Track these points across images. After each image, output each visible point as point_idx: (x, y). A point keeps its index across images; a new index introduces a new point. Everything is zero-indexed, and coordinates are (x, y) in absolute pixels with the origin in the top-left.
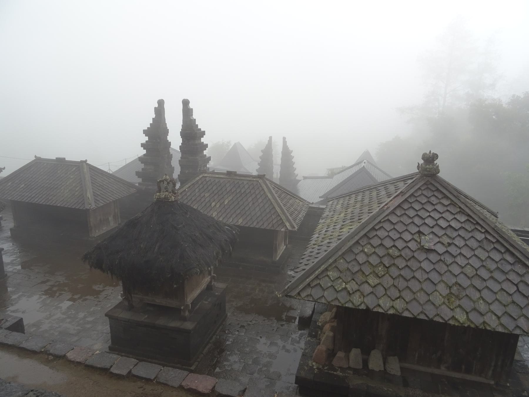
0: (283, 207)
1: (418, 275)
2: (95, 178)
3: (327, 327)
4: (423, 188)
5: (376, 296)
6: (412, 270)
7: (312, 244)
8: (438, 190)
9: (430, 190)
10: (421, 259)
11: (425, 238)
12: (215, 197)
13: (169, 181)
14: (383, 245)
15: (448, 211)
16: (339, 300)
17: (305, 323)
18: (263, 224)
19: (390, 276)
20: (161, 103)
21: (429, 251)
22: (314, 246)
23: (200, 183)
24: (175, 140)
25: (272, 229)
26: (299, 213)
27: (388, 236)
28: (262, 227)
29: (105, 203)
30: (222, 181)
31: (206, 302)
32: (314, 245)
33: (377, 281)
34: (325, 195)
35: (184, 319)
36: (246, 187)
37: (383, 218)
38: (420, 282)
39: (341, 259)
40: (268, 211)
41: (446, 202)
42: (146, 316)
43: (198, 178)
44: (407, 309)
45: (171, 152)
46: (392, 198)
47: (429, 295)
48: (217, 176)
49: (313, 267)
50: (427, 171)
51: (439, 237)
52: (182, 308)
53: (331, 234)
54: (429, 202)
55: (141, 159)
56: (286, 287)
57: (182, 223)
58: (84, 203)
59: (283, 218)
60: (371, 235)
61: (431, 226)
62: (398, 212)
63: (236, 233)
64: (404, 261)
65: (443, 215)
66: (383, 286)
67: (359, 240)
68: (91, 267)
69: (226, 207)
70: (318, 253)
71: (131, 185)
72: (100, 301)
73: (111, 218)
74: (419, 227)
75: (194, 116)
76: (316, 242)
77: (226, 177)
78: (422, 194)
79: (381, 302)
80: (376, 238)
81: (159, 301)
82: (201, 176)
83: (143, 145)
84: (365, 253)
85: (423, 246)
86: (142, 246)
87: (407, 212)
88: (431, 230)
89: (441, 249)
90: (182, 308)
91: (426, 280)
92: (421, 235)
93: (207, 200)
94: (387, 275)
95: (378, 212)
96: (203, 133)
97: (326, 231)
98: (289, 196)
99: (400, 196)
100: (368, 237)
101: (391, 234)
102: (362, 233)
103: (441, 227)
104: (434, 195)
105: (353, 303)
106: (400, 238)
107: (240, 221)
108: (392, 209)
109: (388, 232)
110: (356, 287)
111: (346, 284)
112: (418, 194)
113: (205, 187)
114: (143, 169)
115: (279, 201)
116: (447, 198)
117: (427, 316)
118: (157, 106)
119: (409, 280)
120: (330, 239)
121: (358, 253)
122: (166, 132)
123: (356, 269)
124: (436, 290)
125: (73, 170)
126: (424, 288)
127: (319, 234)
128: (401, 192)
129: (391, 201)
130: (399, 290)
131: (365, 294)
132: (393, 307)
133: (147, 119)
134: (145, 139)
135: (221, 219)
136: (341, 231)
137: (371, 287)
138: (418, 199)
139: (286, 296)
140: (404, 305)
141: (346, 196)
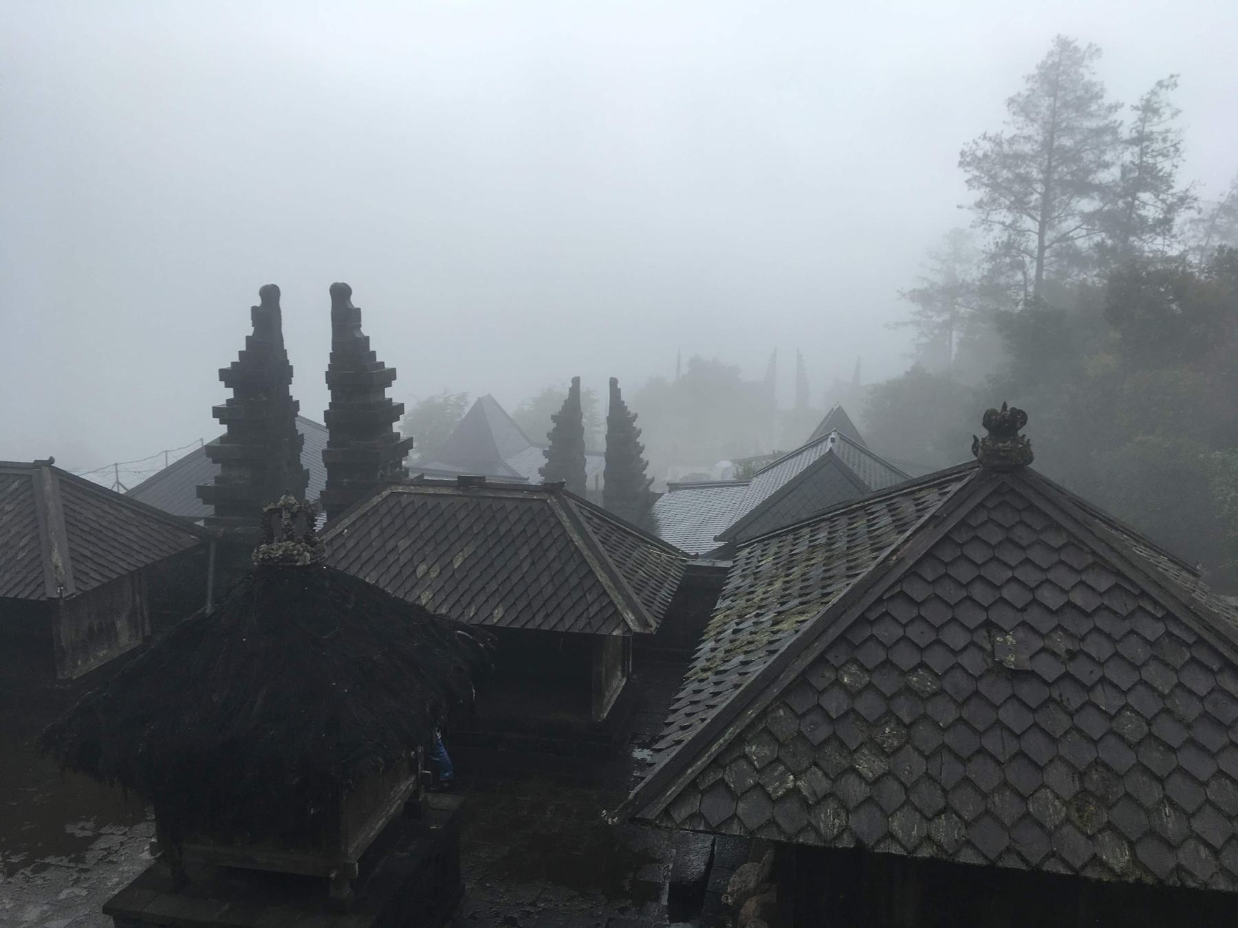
1: (991, 743)
5: (881, 809)
8: (1031, 507)
10: (998, 700)
11: (1005, 641)
14: (892, 665)
15: (1062, 562)
16: (778, 826)
19: (916, 749)
20: (270, 295)
21: (1018, 675)
22: (705, 675)
24: (311, 396)
25: (588, 631)
26: (660, 584)
27: (905, 638)
28: (560, 629)
29: (106, 581)
32: (704, 670)
33: (880, 766)
34: (728, 531)
38: (999, 763)
41: (1057, 540)
43: (377, 500)
44: (968, 843)
45: (300, 428)
48: (431, 491)
51: (1042, 636)
55: (212, 451)
59: (618, 599)
62: (929, 573)
65: (1051, 576)
66: (898, 779)
69: (458, 576)
70: (715, 694)
71: (186, 525)
73: (121, 624)
75: (365, 330)
77: (456, 493)
79: (895, 825)
82: (385, 493)
83: (217, 412)
84: (844, 687)
85: (1001, 662)
89: (1049, 669)
91: (1014, 757)
92: (994, 632)
96: (391, 375)
97: (735, 632)
99: (931, 527)
101: (914, 632)
102: (834, 633)
103: (1047, 608)
104: (1021, 522)
105: (816, 830)
106: (937, 642)
107: (498, 613)
108: (911, 562)
109: (905, 626)
110: (824, 785)
111: (796, 779)
115: (605, 554)
116: (1059, 528)
118: (258, 302)
119: (969, 760)
122: (286, 373)
123: (823, 733)
127: (717, 641)
128: (933, 517)
129: (907, 541)
130: (944, 790)
131: (851, 806)
132: (929, 838)
133: (232, 339)
135: (443, 611)
137: (867, 783)
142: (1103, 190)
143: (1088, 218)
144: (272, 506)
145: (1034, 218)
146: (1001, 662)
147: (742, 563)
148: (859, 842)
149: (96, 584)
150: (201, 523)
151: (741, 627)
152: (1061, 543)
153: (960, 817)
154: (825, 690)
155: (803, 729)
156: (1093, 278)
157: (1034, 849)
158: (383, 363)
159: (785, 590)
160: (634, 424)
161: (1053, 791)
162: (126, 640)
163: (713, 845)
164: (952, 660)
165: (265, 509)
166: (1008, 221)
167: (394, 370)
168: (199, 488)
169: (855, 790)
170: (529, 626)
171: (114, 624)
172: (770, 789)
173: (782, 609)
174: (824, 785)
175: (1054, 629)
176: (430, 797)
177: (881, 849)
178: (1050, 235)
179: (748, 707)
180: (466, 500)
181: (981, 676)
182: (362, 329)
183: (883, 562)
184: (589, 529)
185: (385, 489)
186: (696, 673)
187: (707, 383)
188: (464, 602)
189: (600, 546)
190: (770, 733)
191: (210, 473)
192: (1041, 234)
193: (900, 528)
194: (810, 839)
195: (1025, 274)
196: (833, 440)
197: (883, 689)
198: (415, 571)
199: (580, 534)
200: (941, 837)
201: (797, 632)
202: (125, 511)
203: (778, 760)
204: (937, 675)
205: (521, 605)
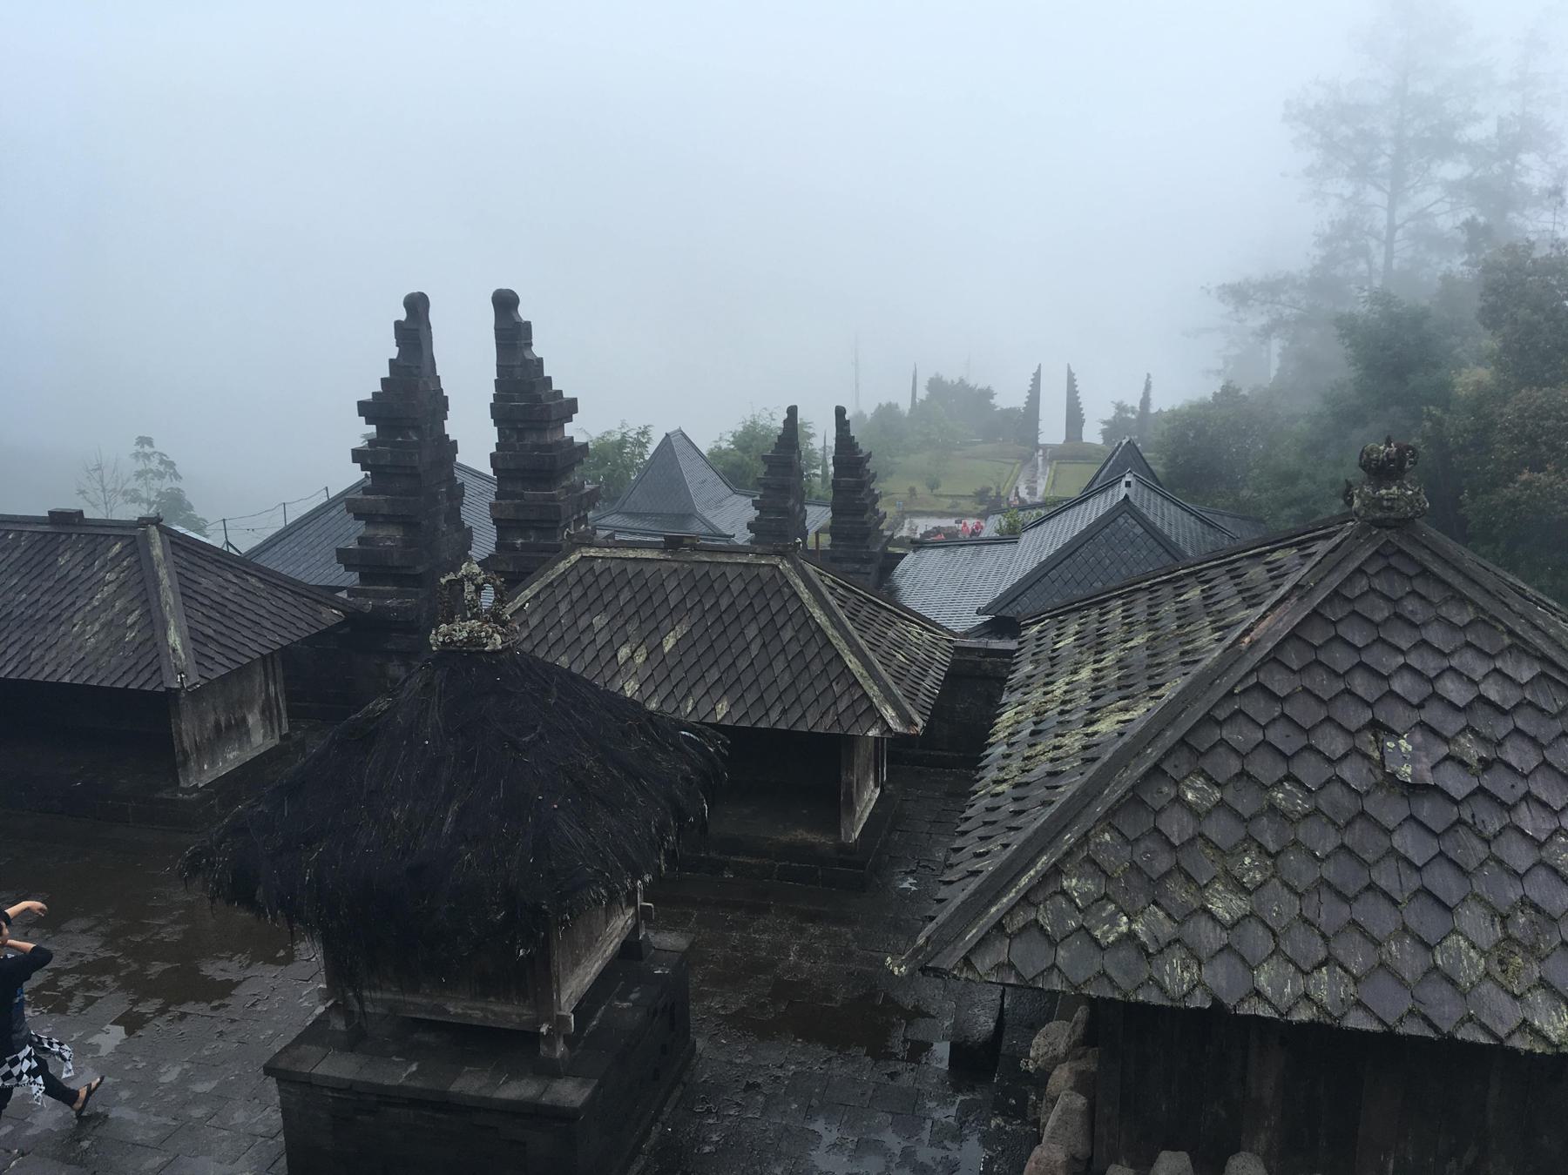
0: (869, 652)
1: (1385, 878)
2: (193, 577)
3: (1061, 1077)
4: (1371, 570)
5: (1243, 959)
6: (1363, 863)
7: (987, 780)
8: (1425, 572)
9: (1400, 573)
10: (1390, 820)
11: (1398, 746)
12: (630, 628)
13: (480, 580)
14: (1250, 777)
15: (1469, 645)
16: (1111, 980)
17: (982, 1064)
18: (803, 716)
19: (1285, 884)
20: (417, 305)
21: (1416, 790)
22: (999, 789)
23: (571, 580)
24: (473, 436)
25: (837, 730)
26: (924, 672)
27: (1264, 743)
28: (802, 728)
29: (234, 666)
30: (649, 570)
31: (625, 1005)
32: (998, 782)
33: (1240, 905)
34: (997, 601)
35: (551, 1071)
36: (736, 588)
37: (1240, 681)
38: (1395, 903)
39: (1103, 831)
40: (816, 668)
41: (1461, 616)
42: (414, 1068)
43: (562, 566)
44: (1359, 1004)
45: (460, 477)
46: (1263, 609)
47: (1429, 948)
48: (631, 554)
49: (1011, 861)
50: (1382, 508)
51: (1447, 741)
52: (544, 1030)
53: (1056, 742)
54: (1398, 616)
55: (351, 503)
56: (921, 941)
57: (534, 728)
58: (159, 668)
59: (873, 691)
60: (1204, 741)
61: (1415, 701)
62: (1293, 659)
63: (717, 751)
64: (1331, 829)
65: (1454, 662)
66: (1264, 923)
67: (1161, 760)
68: (213, 899)
69: (670, 662)
70: (1017, 813)
71: (327, 593)
72: (233, 1021)
73: (253, 719)
74: (1369, 705)
75: (538, 350)
76: (1002, 775)
77: (662, 557)
78: (1372, 590)
79: (1262, 980)
80: (1221, 750)
81: (458, 1008)
82: (574, 558)
83: (358, 456)
84: (1189, 807)
85: (1393, 775)
86: (396, 815)
87: (1322, 658)
88: (1416, 716)
89: (1457, 783)
90: (544, 1030)
91: (1415, 894)
92: (1382, 736)
93: (600, 641)
94: (1275, 880)
95: (1220, 662)
96: (571, 407)
97: (1033, 733)
98: (884, 613)
99: (1294, 600)
100: (1191, 748)
101: (1276, 735)
102: (1171, 736)
103: (1452, 705)
104: (1413, 593)
105: (1162, 989)
106: (1309, 748)
107: (722, 709)
108: (1270, 645)
109: (1264, 728)
110: (1168, 929)
111: (1131, 921)
112: (1357, 592)
113: (592, 594)
114: (361, 540)
115: (856, 634)
116: (1464, 600)
117: (1431, 1025)
118: (402, 315)
119: (1356, 898)
120: (1052, 760)
121: (1162, 809)
122: (440, 405)
123: (1163, 863)
124: (1454, 931)
125: (110, 555)
126: (1412, 923)
127: (1010, 745)
128: (1296, 586)
129: (1263, 617)
130: (1323, 936)
131: (1204, 956)
132: (1307, 996)
133: (371, 362)
134: (361, 432)
135: (653, 705)
136: (1090, 730)
137: (1224, 927)
138: (1358, 608)
139: (924, 970)
140: (1346, 990)
141: (1089, 607)
142: (1470, 149)
143: (1452, 188)
144: (451, 576)
145: (1379, 188)
146: (1393, 775)
147: (1031, 647)
148: (1217, 1003)
149: (224, 671)
150: (343, 595)
151: (1040, 727)
152: (1467, 620)
153: (1346, 971)
154: (1162, 809)
155: (1136, 859)
156: (1459, 265)
157: (1446, 1013)
158: (560, 392)
159: (1096, 680)
160: (868, 466)
161: (1467, 939)
162: (260, 740)
163: (1002, 997)
164: (1328, 772)
165: (443, 581)
166: (1348, 193)
167: (575, 400)
168: (339, 551)
169: (1209, 937)
170: (762, 725)
171: (244, 720)
172: (1098, 933)
173: (1095, 705)
174: (1168, 929)
175: (1462, 732)
176: (651, 935)
177: (1246, 1009)
178: (1403, 211)
179: (1066, 828)
180: (675, 565)
181: (1368, 792)
182: (533, 348)
183: (1231, 646)
184: (834, 603)
185: (573, 551)
186: (986, 786)
187: (958, 408)
188: (679, 693)
189: (848, 623)
190: (1094, 862)
191: (352, 532)
192: (1391, 210)
193: (1252, 601)
194: (1152, 997)
195: (1369, 263)
196: (1128, 484)
197: (1239, 808)
198: (616, 655)
199: (822, 608)
200: (1323, 995)
201: (1121, 734)
202: (253, 580)
203: (1106, 897)
204: (1309, 790)
205: (751, 698)
